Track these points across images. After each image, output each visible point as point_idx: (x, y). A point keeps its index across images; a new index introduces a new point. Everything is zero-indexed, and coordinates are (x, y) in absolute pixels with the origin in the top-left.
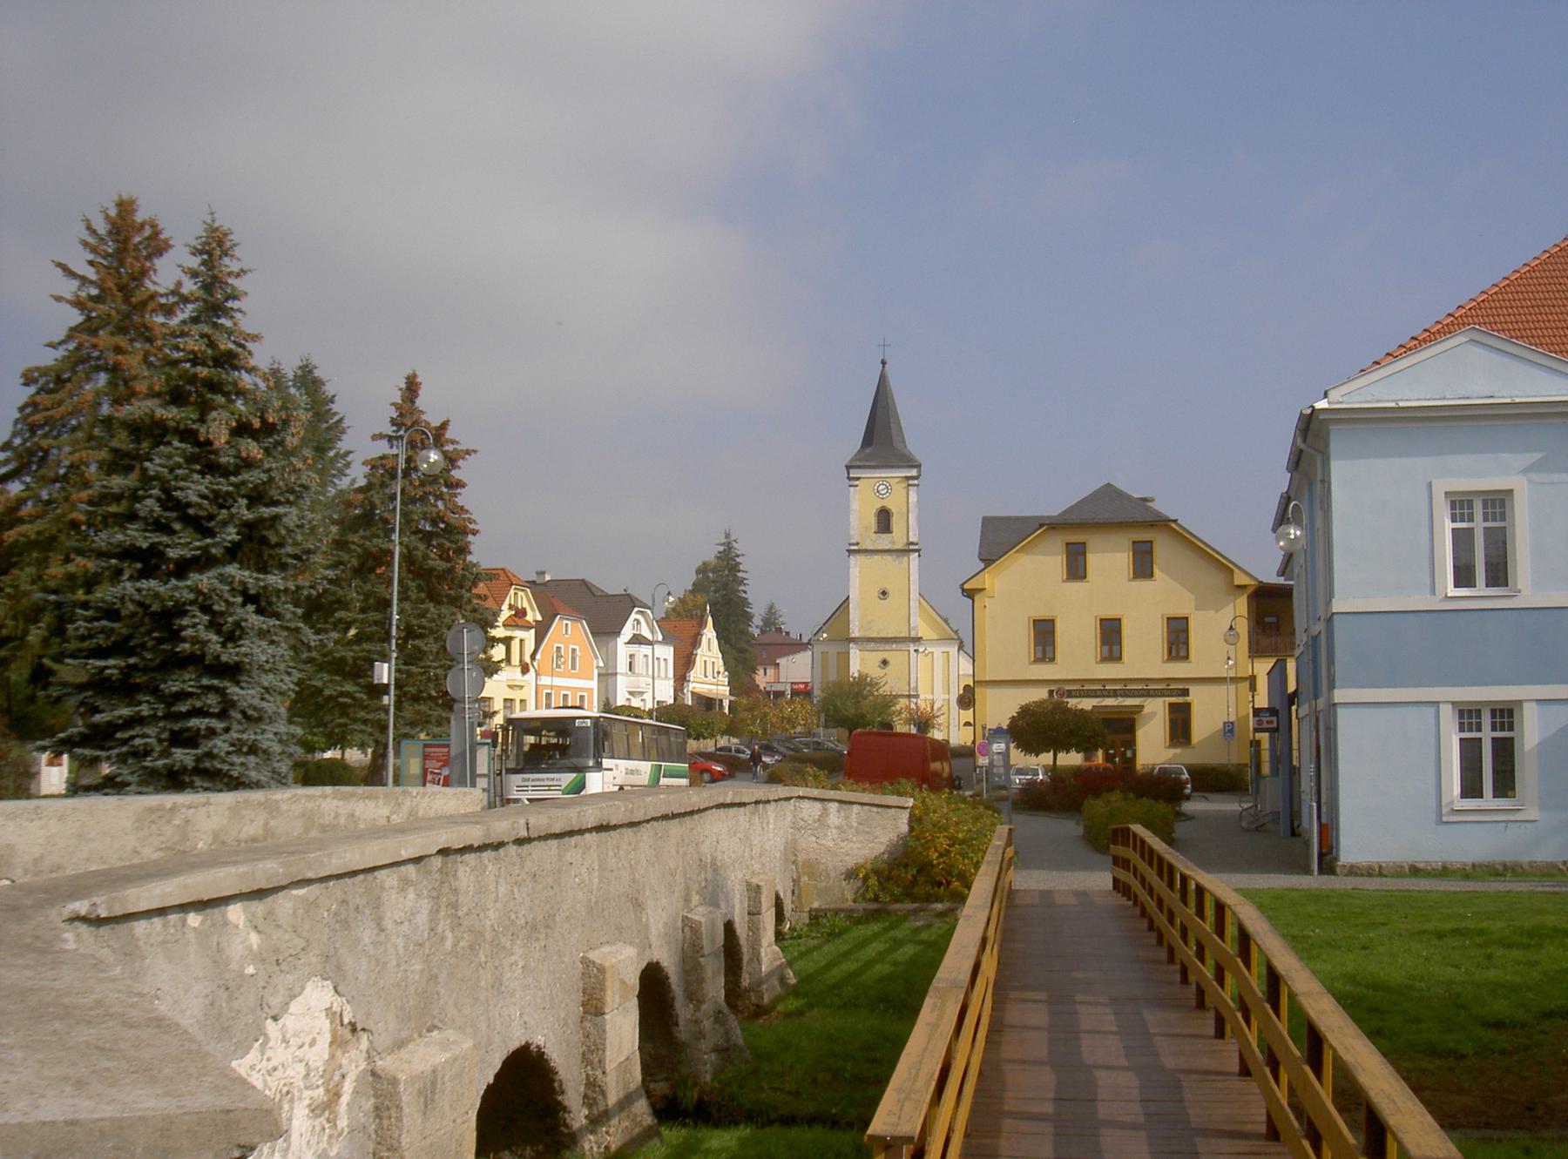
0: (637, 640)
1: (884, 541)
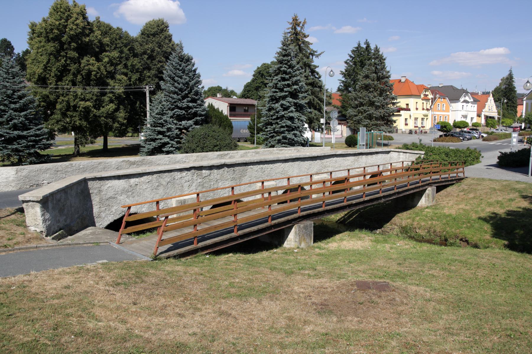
0: (466, 102)
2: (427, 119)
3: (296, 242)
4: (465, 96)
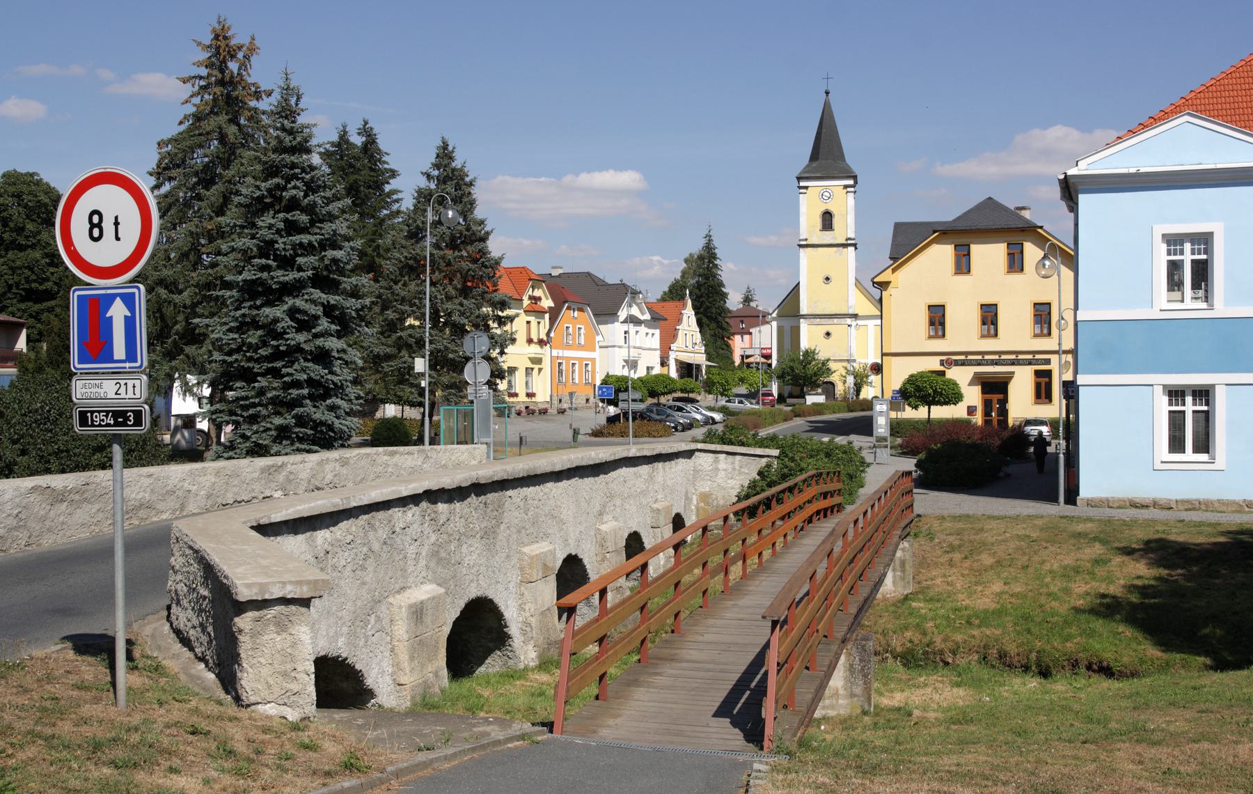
0: (632, 320)
1: (827, 237)
2: (540, 370)
3: (852, 695)
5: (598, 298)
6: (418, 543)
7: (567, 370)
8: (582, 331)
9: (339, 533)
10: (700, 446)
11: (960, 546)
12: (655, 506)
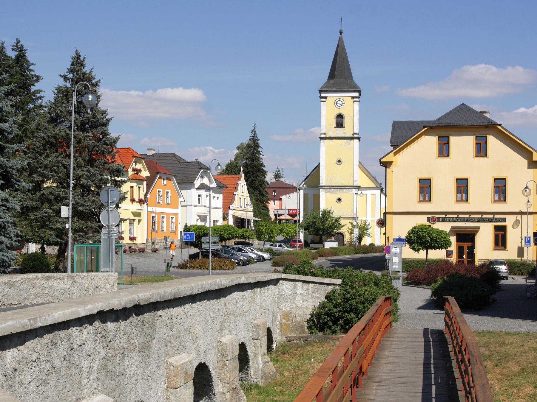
0: (203, 187)
1: (340, 132)
2: (140, 221)
4: (202, 177)
5: (181, 172)
6: (91, 358)
7: (158, 222)
8: (170, 194)
9: (26, 352)
10: (283, 276)
11: (490, 356)
12: (256, 322)
